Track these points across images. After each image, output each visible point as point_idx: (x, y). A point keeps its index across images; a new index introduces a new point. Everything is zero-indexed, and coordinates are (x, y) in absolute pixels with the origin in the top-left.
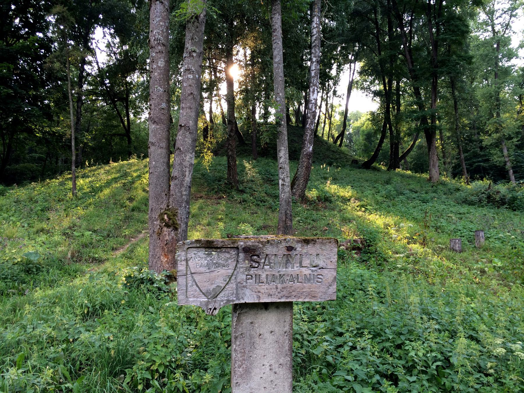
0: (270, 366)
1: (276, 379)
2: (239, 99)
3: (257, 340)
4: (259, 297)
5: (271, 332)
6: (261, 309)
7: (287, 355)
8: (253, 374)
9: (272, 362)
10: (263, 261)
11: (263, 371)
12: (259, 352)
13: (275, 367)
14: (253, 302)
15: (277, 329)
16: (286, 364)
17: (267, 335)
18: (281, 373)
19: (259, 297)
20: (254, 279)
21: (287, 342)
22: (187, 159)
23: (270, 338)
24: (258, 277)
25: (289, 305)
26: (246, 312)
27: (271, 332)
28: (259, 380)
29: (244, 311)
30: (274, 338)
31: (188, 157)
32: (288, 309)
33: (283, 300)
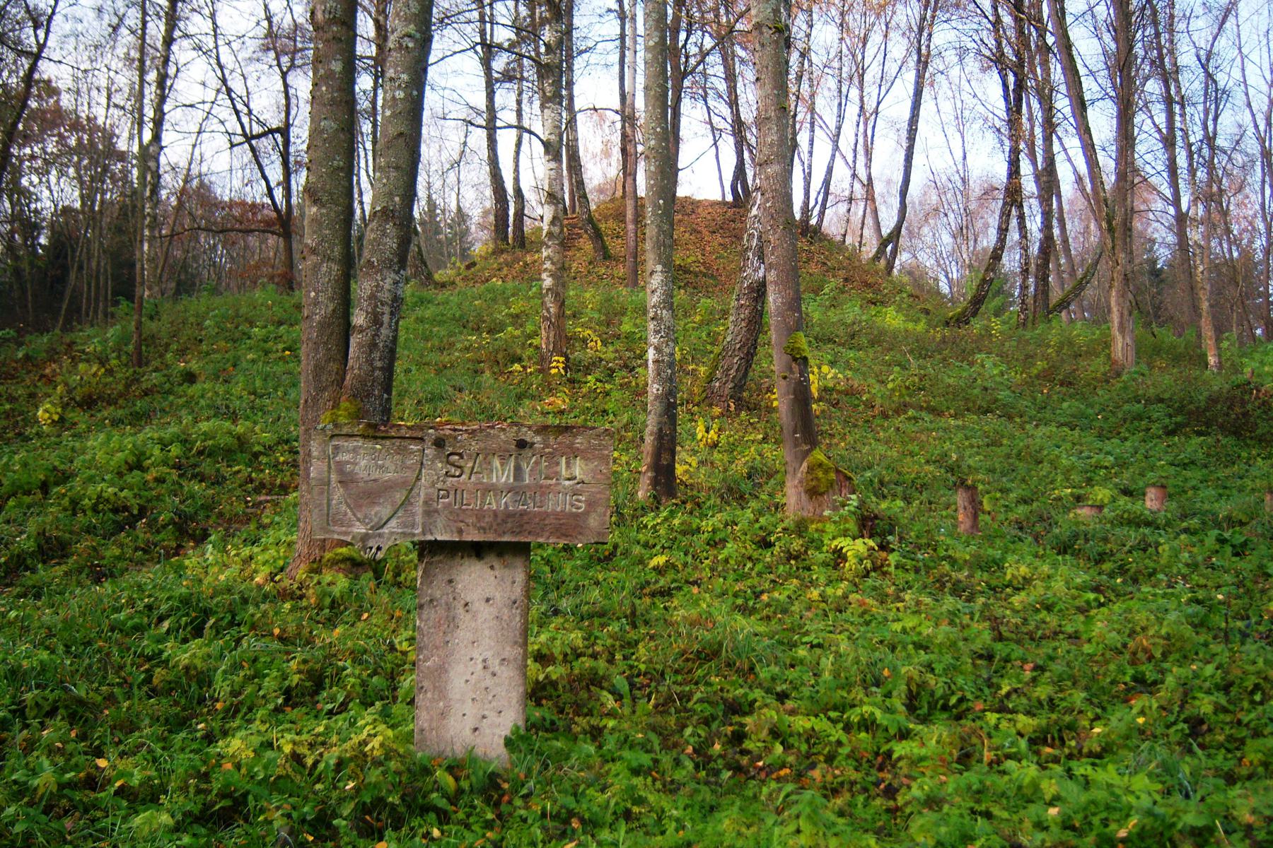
0: (484, 661)
1: (497, 685)
2: (1030, 301)
3: (460, 611)
4: (460, 531)
5: (488, 600)
6: (470, 556)
7: (516, 643)
8: (452, 674)
9: (488, 654)
10: (470, 464)
11: (471, 670)
12: (463, 635)
13: (495, 664)
14: (426, 106)
15: (498, 595)
16: (515, 659)
17: (478, 605)
18: (505, 675)
19: (460, 531)
20: (452, 496)
21: (518, 619)
22: (387, 286)
23: (485, 612)
24: (459, 492)
25: (522, 550)
26: (440, 562)
27: (488, 600)
28: (463, 684)
29: (436, 559)
30: (494, 611)
31: (388, 281)
32: (519, 562)
33: (506, 539)
